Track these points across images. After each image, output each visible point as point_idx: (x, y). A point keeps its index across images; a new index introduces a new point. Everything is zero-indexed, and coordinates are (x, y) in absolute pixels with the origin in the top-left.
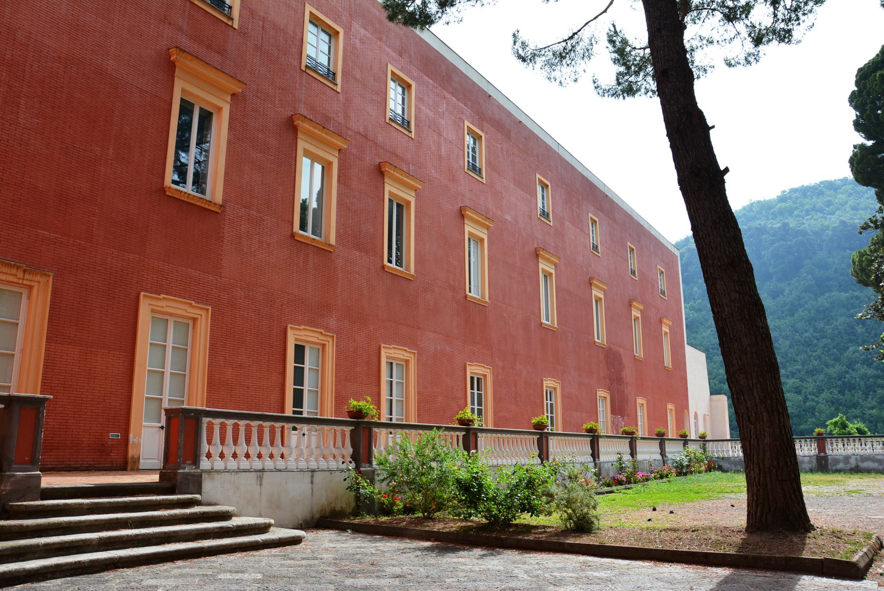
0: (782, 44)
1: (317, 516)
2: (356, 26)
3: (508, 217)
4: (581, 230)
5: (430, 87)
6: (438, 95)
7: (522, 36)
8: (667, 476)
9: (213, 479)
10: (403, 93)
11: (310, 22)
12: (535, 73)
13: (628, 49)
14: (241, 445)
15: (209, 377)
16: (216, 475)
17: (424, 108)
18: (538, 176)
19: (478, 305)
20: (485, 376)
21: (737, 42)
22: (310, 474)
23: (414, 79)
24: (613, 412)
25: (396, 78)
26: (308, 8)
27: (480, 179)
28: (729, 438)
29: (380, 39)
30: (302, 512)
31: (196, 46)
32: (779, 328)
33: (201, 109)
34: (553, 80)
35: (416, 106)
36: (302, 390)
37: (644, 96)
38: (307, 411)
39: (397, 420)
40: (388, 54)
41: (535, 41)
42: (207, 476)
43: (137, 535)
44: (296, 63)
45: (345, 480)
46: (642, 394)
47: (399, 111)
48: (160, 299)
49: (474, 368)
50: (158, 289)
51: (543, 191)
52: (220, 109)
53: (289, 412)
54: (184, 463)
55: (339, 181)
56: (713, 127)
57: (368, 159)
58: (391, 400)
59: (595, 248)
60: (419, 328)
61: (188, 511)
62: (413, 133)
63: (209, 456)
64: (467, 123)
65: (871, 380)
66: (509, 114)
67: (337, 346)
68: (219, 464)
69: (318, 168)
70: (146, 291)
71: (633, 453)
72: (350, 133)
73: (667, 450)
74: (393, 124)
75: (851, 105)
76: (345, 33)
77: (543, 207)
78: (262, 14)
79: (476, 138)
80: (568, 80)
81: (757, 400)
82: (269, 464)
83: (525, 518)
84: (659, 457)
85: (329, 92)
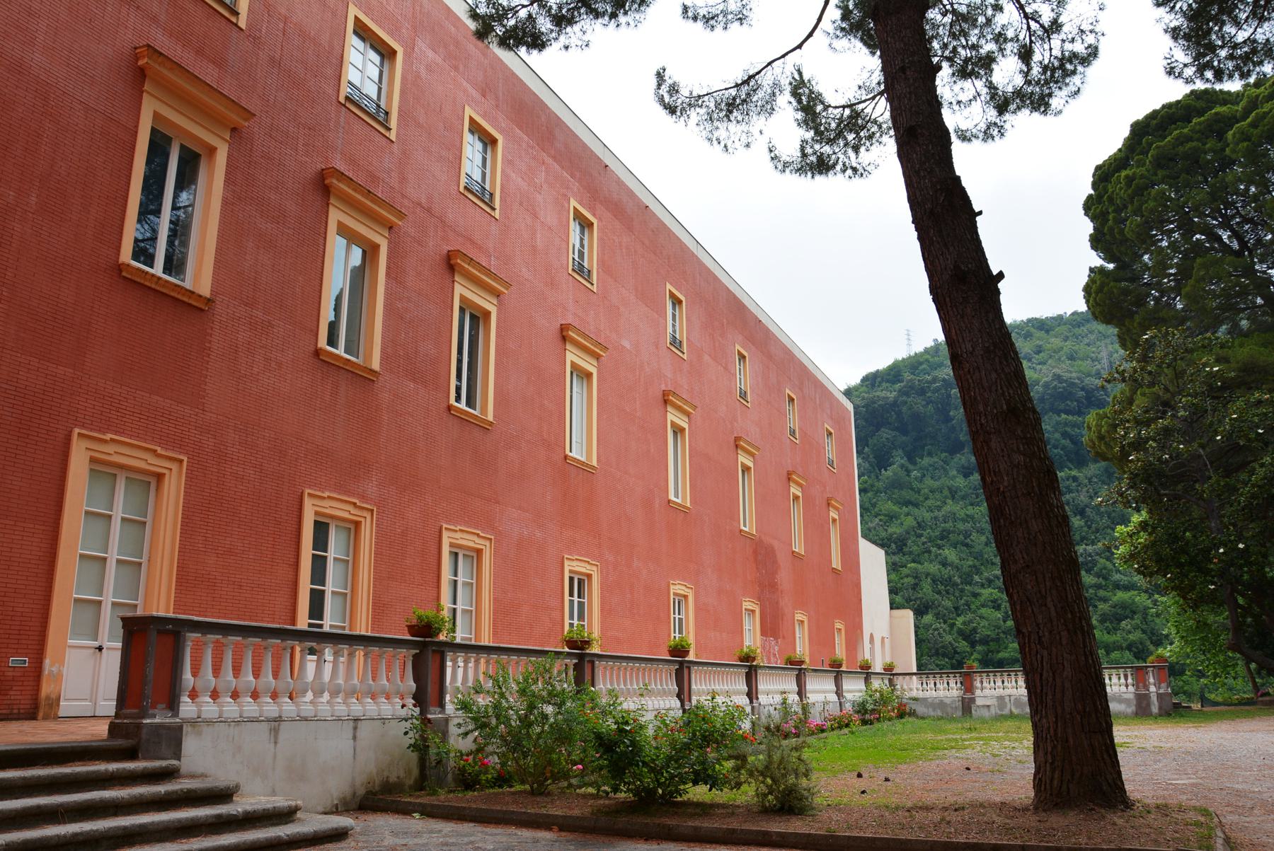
0: (1036, 115)
1: (361, 792)
2: (421, 45)
3: (626, 344)
4: (726, 369)
5: (524, 145)
6: (534, 158)
7: (672, 75)
8: (847, 725)
9: (199, 734)
10: (485, 151)
11: (355, 32)
12: (689, 130)
13: (819, 108)
14: (267, 677)
15: (181, 568)
16: (206, 729)
17: (513, 175)
18: (669, 287)
19: (582, 467)
20: (589, 576)
21: (977, 106)
22: (351, 723)
23: (501, 131)
24: (763, 633)
25: (475, 128)
26: (353, 11)
27: (589, 285)
28: (915, 670)
29: (456, 68)
30: (337, 787)
31: (179, 49)
32: (972, 517)
33: (183, 147)
34: (715, 142)
35: (503, 171)
36: (323, 592)
37: (840, 176)
38: (329, 622)
39: (463, 639)
40: (465, 91)
41: (691, 81)
42: (190, 729)
43: (75, 835)
44: (330, 91)
45: (406, 733)
46: (801, 604)
47: (477, 176)
48: (105, 441)
49: (575, 563)
50: (106, 420)
51: (674, 309)
52: (212, 151)
53: (303, 623)
54: (154, 707)
55: (388, 274)
56: (980, 213)
57: (431, 244)
58: (455, 610)
59: (743, 395)
60: (497, 502)
61: (161, 789)
62: (497, 212)
63: (193, 695)
64: (573, 203)
65: (1091, 591)
66: (631, 194)
67: (378, 526)
68: (209, 708)
69: (357, 253)
70: (83, 427)
71: (801, 693)
72: (406, 202)
73: (845, 687)
74: (470, 196)
75: (1086, 214)
76: (405, 54)
77: (674, 331)
78: (283, 11)
79: (585, 225)
80: (737, 144)
81: (1053, 614)
82: (288, 707)
83: (699, 793)
84: (834, 698)
85: (378, 138)
